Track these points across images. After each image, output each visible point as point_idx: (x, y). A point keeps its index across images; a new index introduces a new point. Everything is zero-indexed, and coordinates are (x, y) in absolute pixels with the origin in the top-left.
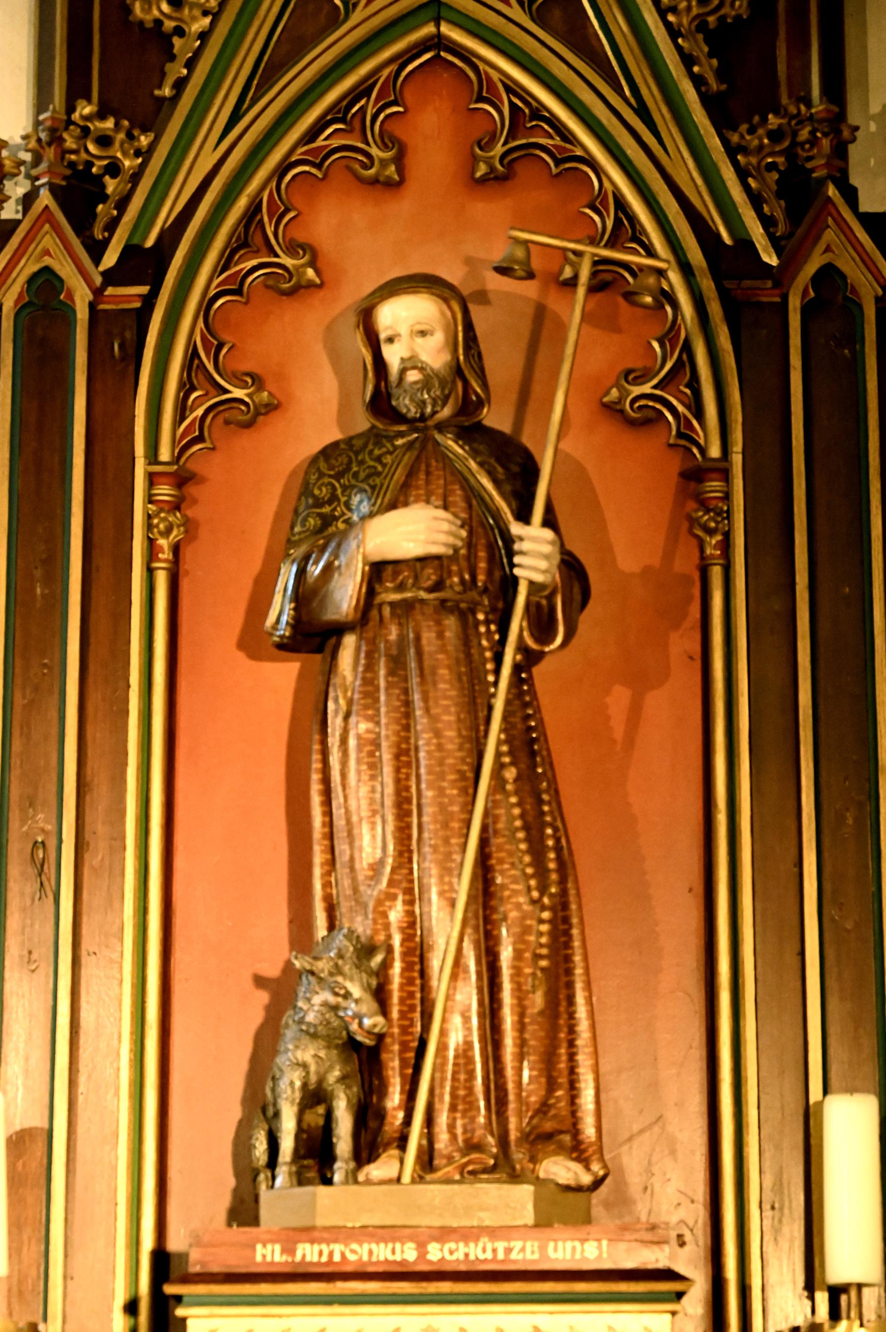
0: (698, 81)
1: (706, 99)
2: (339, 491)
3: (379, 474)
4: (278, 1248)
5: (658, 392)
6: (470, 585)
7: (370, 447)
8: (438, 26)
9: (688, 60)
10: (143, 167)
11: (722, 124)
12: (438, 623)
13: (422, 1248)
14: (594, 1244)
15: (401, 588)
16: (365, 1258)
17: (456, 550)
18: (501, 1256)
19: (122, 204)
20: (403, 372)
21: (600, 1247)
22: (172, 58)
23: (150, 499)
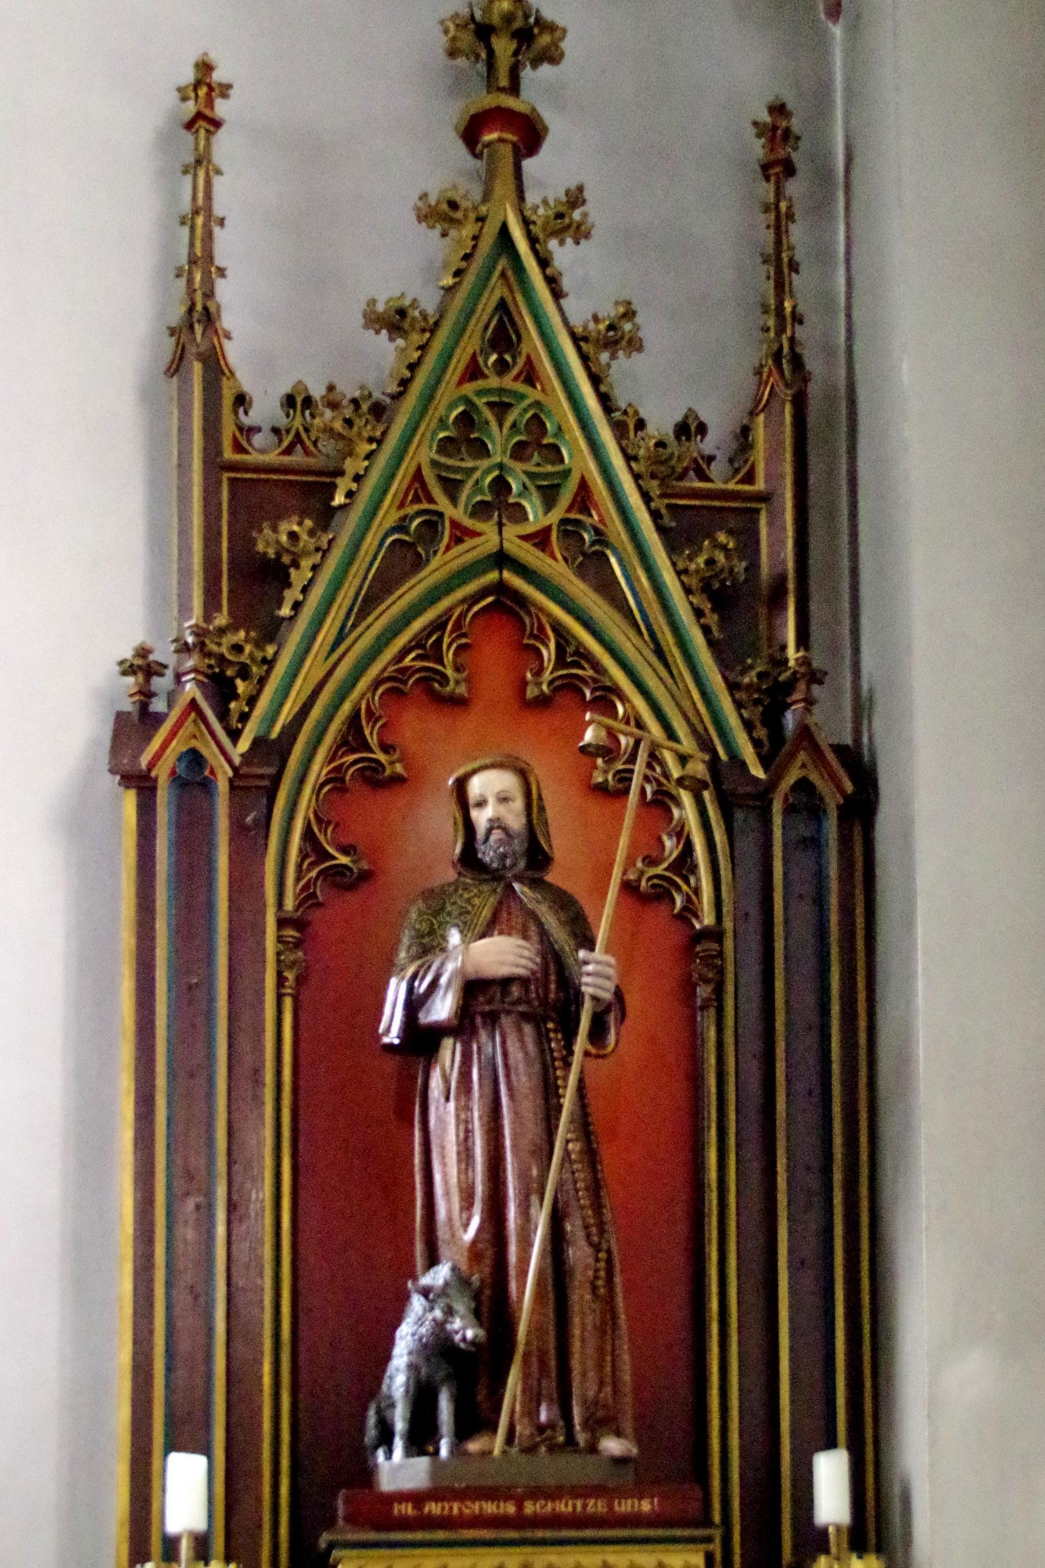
0: (706, 630)
1: (711, 643)
2: (436, 927)
3: (468, 913)
4: (410, 1506)
5: (667, 874)
6: (544, 1001)
7: (460, 892)
8: (501, 573)
9: (698, 613)
10: (269, 672)
11: (724, 665)
12: (520, 1030)
13: (520, 1507)
14: (648, 1500)
15: (489, 1002)
16: (477, 1511)
17: (533, 973)
18: (579, 1508)
19: (252, 701)
20: (489, 832)
21: (652, 1503)
22: (289, 585)
23: (280, 939)
